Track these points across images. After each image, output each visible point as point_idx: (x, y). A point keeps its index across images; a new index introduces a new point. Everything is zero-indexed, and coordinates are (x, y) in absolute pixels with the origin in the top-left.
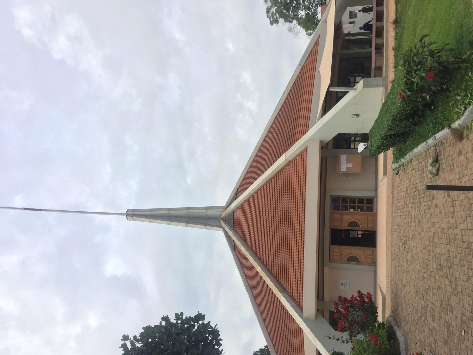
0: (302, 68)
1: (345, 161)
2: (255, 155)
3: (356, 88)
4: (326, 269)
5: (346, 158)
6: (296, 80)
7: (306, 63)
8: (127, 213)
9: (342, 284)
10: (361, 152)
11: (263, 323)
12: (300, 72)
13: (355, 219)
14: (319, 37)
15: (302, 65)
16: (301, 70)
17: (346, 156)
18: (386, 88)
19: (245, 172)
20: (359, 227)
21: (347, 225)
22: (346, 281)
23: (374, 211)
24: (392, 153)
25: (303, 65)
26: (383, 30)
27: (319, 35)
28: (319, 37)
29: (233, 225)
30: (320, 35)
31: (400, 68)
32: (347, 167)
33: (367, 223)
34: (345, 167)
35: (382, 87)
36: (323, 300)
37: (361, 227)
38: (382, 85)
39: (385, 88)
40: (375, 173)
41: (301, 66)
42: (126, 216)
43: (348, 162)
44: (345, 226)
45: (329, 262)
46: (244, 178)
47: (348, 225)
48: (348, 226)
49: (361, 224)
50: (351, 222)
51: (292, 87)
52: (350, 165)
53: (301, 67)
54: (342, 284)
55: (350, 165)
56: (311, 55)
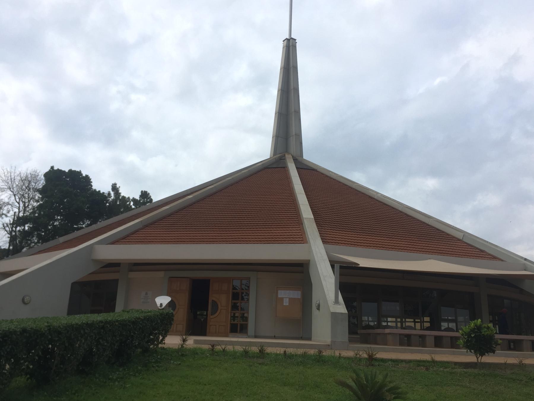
0: (459, 240)
1: (291, 297)
2: (354, 187)
3: (338, 303)
4: (161, 274)
5: (296, 297)
6: (443, 232)
7: (466, 245)
8: (291, 39)
9: (146, 294)
10: (155, 301)
11: (148, 209)
12: (454, 237)
13: (221, 309)
14: (502, 261)
15: (464, 240)
16: (456, 238)
17: (300, 298)
18: (328, 347)
19: (334, 178)
20: (211, 315)
21: (214, 299)
22: (150, 299)
23: (230, 334)
24: (191, 347)
25: (464, 242)
26: (456, 349)
27: (505, 260)
28: (502, 261)
29: (273, 167)
30: (505, 261)
31: (151, 346)
32: (284, 299)
33: (216, 325)
34: (284, 297)
35: (332, 341)
36: (131, 271)
37: (212, 317)
38: (335, 341)
39: (329, 345)
40: (275, 336)
41: (463, 238)
42: (287, 39)
43: (291, 300)
44: (213, 297)
45: (170, 277)
46: (327, 176)
47: (214, 301)
48: (213, 300)
49: (215, 317)
50: (218, 305)
51: (434, 227)
52: (286, 303)
53: (461, 239)
54: (146, 294)
55: (286, 303)
56: (477, 250)
